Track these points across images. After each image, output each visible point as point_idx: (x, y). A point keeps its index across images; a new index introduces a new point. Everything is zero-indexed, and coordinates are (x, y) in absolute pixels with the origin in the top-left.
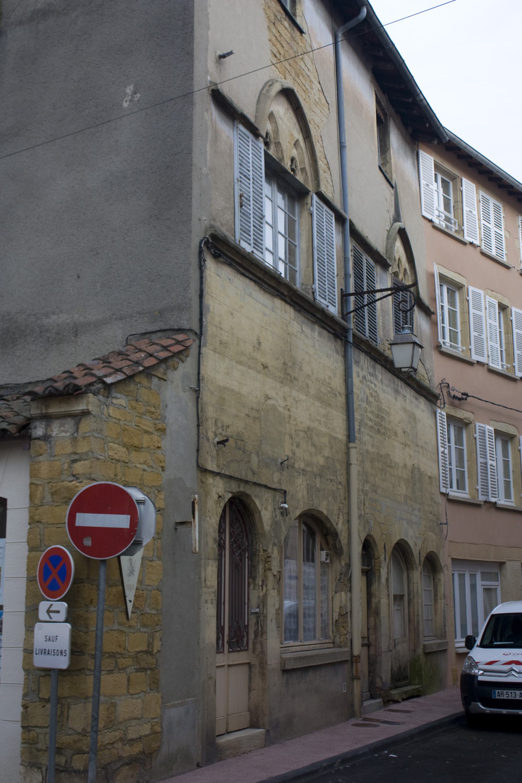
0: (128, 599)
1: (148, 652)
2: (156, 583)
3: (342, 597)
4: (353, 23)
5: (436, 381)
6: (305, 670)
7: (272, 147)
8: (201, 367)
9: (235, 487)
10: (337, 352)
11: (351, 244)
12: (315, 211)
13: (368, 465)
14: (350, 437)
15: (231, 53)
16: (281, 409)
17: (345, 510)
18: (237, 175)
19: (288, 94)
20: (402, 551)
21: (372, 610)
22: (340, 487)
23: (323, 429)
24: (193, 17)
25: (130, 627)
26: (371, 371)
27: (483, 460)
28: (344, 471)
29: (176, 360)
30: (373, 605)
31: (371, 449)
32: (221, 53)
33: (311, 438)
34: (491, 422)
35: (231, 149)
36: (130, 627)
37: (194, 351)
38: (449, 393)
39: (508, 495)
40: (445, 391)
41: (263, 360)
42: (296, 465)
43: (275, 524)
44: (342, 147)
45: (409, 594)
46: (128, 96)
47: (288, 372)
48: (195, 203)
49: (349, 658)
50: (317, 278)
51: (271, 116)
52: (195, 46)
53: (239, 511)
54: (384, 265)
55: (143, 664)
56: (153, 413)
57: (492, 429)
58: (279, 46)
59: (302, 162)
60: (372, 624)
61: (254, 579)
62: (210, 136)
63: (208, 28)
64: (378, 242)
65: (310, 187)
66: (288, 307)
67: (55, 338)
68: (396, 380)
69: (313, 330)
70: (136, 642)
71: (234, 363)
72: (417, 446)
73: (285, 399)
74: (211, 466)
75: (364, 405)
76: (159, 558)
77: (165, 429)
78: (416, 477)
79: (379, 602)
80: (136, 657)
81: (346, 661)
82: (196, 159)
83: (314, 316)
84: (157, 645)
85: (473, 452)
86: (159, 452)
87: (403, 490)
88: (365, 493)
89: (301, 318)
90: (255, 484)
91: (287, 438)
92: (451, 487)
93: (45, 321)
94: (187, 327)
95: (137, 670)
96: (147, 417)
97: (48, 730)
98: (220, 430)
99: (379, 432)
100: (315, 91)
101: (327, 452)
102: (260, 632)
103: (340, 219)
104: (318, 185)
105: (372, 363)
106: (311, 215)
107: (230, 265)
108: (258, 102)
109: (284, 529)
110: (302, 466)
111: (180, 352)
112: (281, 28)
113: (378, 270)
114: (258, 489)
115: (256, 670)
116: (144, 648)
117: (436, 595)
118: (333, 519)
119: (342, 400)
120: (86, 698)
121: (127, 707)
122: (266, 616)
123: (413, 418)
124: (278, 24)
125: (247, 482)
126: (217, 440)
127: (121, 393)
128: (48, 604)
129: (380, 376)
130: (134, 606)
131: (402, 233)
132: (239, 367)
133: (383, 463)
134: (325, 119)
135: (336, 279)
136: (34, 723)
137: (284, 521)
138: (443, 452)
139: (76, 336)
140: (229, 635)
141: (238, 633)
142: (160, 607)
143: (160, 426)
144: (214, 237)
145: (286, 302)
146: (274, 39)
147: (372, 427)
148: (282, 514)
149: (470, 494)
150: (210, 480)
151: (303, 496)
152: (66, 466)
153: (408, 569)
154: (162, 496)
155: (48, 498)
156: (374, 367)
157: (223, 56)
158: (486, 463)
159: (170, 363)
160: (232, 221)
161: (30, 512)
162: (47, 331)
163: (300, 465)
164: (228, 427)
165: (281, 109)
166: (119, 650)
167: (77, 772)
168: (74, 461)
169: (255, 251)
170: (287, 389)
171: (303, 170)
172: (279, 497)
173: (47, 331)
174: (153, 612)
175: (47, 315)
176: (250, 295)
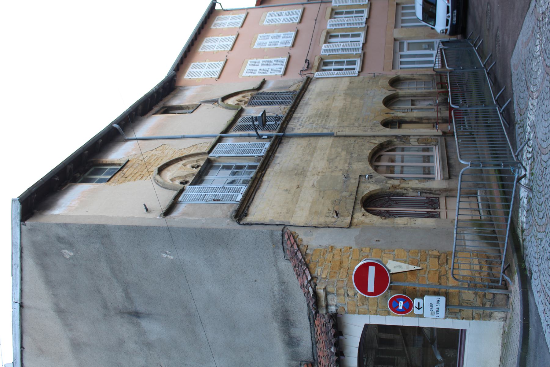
0: (413, 269)
1: (439, 258)
2: (406, 253)
3: (413, 141)
4: (121, 131)
5: (299, 78)
6: (449, 166)
7: (187, 179)
8: (300, 225)
9: (359, 206)
10: (288, 142)
11: (232, 133)
12: (218, 155)
13: (345, 124)
14: (331, 135)
15: (145, 205)
16: (319, 177)
17: (368, 138)
18: (204, 202)
19: (160, 170)
20: (389, 102)
21: (419, 121)
22: (357, 142)
23: (328, 152)
24: (129, 226)
25: (426, 268)
26: (296, 120)
27: (340, 51)
28: (349, 139)
29: (297, 240)
30: (417, 120)
31: (337, 122)
32: (145, 210)
33: (333, 159)
34: (320, 45)
35: (191, 205)
36: (426, 268)
37: (292, 229)
38: (305, 70)
39: (358, 35)
40: (305, 73)
41: (295, 188)
42: (347, 168)
43: (377, 182)
44: (183, 137)
45: (411, 97)
46: (168, 256)
47: (300, 173)
48: (220, 227)
49: (443, 138)
50: (251, 155)
51: (172, 180)
52: (143, 225)
53: (370, 203)
54: (241, 111)
55: (445, 261)
56: (324, 253)
57: (324, 45)
58: (137, 175)
59: (193, 161)
60: (426, 121)
61: (404, 194)
62: (186, 217)
63: (133, 217)
64: (231, 114)
65: (206, 157)
66: (267, 172)
67: (286, 293)
68: (300, 104)
69: (278, 157)
70: (433, 264)
71: (297, 205)
72: (334, 91)
73: (313, 175)
74: (348, 220)
75: (314, 126)
76: (393, 251)
77: (332, 247)
78: (350, 93)
79: (415, 117)
80: (440, 265)
81: (445, 139)
82: (198, 225)
83: (271, 156)
84: (436, 253)
85: (336, 56)
86: (343, 250)
87: (357, 101)
88: (360, 125)
89: (272, 164)
90: (356, 194)
91: (333, 174)
92: (354, 69)
93: (277, 296)
94: (281, 232)
95: (447, 264)
96: (326, 256)
97: (474, 310)
98: (331, 214)
99: (328, 116)
100: (156, 153)
101: (339, 150)
102: (430, 191)
103: (220, 140)
104: (204, 153)
105: (292, 120)
106: (219, 157)
107: (249, 207)
108: (166, 188)
109: (378, 177)
110: (347, 165)
111: (294, 237)
112: (128, 173)
113: (244, 115)
114: (359, 192)
115: (449, 194)
116: (437, 260)
117: (411, 79)
118: (373, 146)
119: (312, 139)
120: (459, 292)
121: (464, 271)
122: (422, 189)
123: (320, 94)
124: (127, 175)
125: (356, 199)
126: (335, 216)
127: (315, 271)
128: (415, 309)
129: (299, 115)
130: (417, 266)
131: (224, 99)
132: (299, 203)
133: (344, 112)
134: (170, 148)
135: (251, 143)
136: (471, 315)
137: (375, 176)
138: (337, 74)
139: (285, 283)
140: (431, 208)
141: (430, 203)
142: (417, 251)
143: (330, 250)
144: (236, 217)
145: (264, 174)
146: (134, 178)
147: (325, 121)
148: (371, 178)
149: (358, 58)
150: (355, 221)
151: (362, 165)
152: (350, 299)
153: (398, 97)
154: (364, 249)
155: (365, 307)
156: (295, 118)
157: (147, 210)
158: (342, 49)
159: (299, 243)
160: (227, 205)
161: (371, 314)
162: (282, 295)
163: (346, 166)
164: (329, 209)
165: (168, 174)
166: (437, 274)
167: (494, 297)
168: (348, 295)
169: (241, 192)
170: (309, 174)
171: (197, 161)
172: (363, 179)
173: (282, 295)
174: (419, 255)
175: (274, 296)
176: (263, 195)
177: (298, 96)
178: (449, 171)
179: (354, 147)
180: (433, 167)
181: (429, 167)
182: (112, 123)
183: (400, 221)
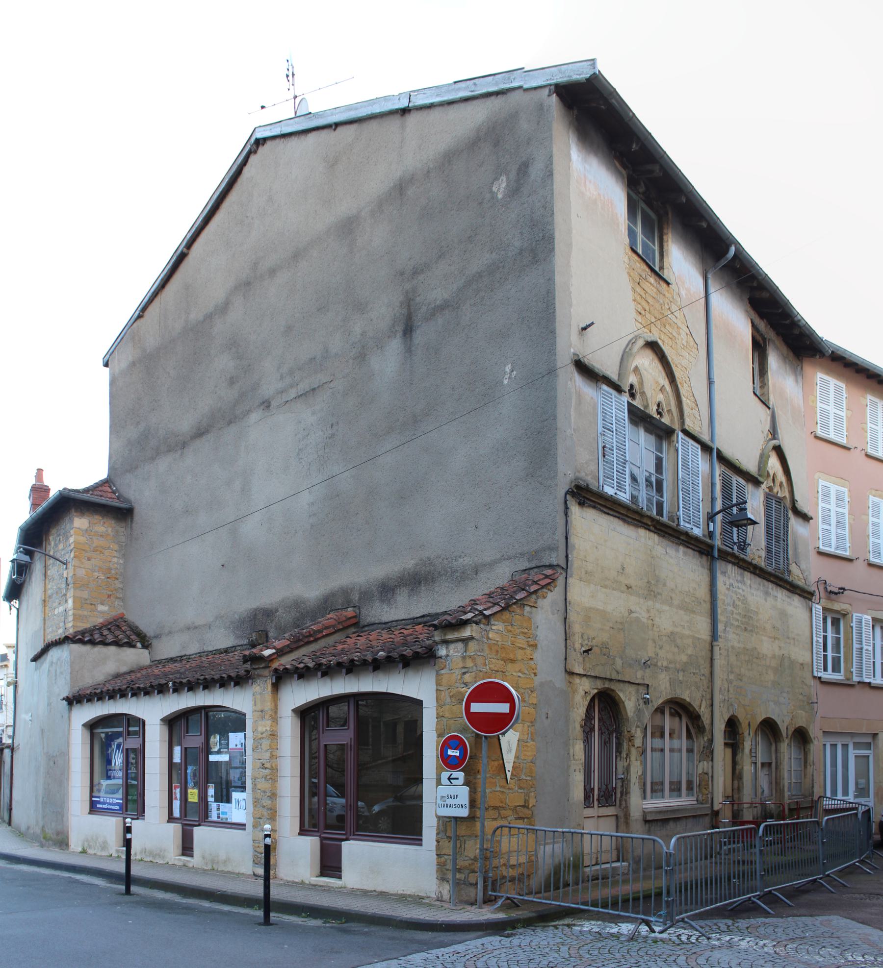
9: (600, 685)
42: (659, 664)
43: (639, 711)
53: (606, 704)
84: (532, 802)
99: (746, 629)
110: (665, 664)
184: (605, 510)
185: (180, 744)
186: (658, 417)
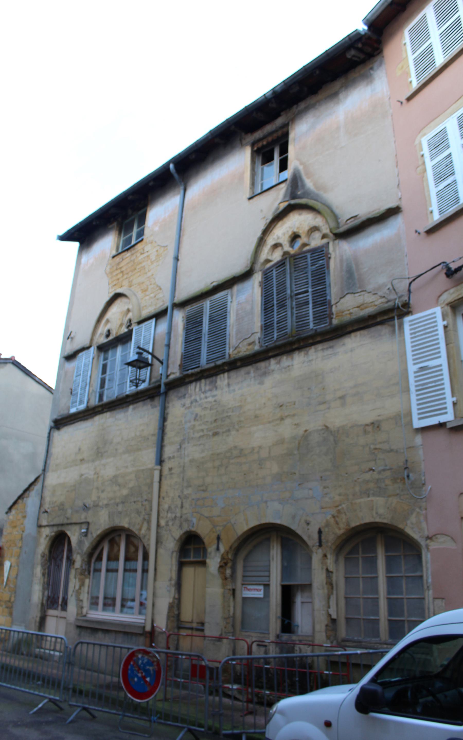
1: (9, 601)
9: (55, 529)
42: (101, 504)
43: (80, 542)
53: (59, 540)
84: (13, 599)
99: (216, 434)
101: (131, 485)
110: (105, 502)
177: (299, 340)
178: (87, 628)
179: (135, 502)
180: (114, 611)
181: (114, 605)
182: (168, 164)
183: (38, 571)
184: (72, 422)
185: (9, 560)
186: (288, 182)
